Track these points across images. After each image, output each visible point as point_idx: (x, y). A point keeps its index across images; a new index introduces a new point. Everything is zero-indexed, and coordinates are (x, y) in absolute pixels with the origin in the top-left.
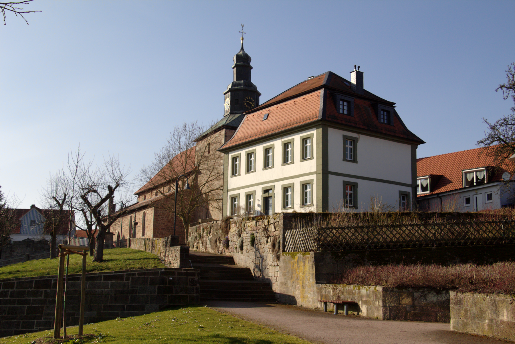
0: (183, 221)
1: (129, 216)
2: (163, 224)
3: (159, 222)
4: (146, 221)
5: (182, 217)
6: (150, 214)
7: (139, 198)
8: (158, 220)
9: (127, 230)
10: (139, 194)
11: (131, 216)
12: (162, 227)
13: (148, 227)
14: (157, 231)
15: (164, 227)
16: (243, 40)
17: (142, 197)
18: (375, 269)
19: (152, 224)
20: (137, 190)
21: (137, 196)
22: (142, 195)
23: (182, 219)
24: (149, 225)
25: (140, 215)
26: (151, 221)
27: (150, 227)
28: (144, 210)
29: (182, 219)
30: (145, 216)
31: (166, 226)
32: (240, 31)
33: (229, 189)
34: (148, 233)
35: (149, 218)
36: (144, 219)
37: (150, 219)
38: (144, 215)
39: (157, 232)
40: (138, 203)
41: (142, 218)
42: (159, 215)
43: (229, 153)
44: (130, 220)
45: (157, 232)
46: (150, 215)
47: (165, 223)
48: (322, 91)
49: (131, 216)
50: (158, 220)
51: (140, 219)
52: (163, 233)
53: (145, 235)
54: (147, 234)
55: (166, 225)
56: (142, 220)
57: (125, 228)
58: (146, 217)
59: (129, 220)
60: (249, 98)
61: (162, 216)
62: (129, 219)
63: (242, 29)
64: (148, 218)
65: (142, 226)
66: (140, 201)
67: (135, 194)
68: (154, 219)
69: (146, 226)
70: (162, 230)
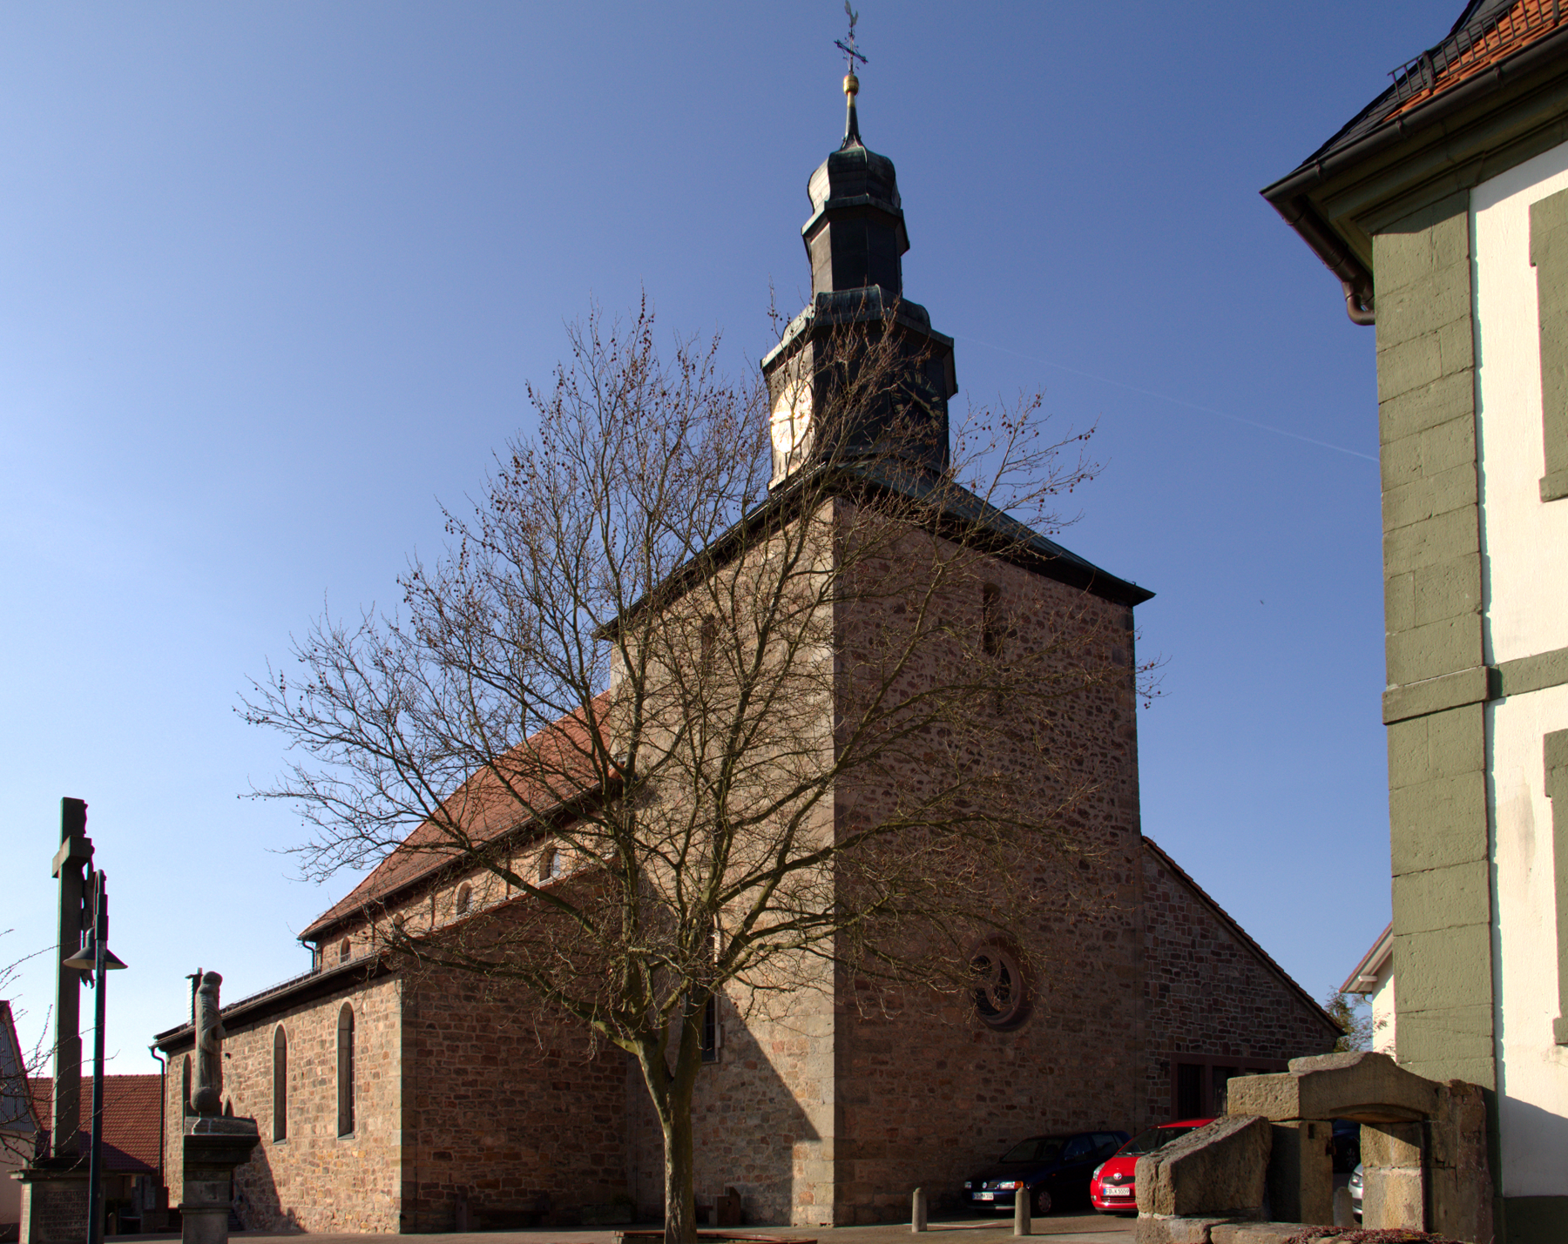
0: (645, 1069)
1: (273, 1027)
2: (459, 1072)
3: (433, 1060)
4: (357, 1056)
5: (639, 1037)
6: (378, 1020)
7: (321, 951)
8: (430, 1053)
9: (262, 1094)
10: (319, 936)
11: (280, 1029)
12: (451, 1089)
13: (373, 1092)
14: (427, 1112)
15: (462, 1091)
16: (854, 90)
17: (333, 949)
18: (1357, 1175)
19: (394, 1074)
20: (308, 918)
21: (313, 945)
22: (331, 941)
23: (638, 1050)
24: (376, 1075)
25: (326, 1023)
26: (386, 1056)
27: (381, 1088)
28: (346, 999)
29: (638, 1050)
30: (351, 1028)
31: (473, 1083)
32: (842, 41)
33: (1501, 656)
34: (370, 1120)
35: (374, 1040)
36: (346, 1043)
37: (382, 1046)
38: (346, 1025)
39: (423, 1117)
40: (315, 973)
41: (336, 1037)
42: (431, 1026)
43: (1478, 192)
44: (277, 1049)
45: (423, 1117)
46: (381, 1025)
47: (469, 1068)
48: (512, 886)
49: (280, 1029)
50: (430, 1053)
51: (323, 1043)
52: (460, 1122)
53: (357, 1128)
54: (365, 1127)
55: (470, 1078)
56: (336, 1047)
57: (257, 1084)
58: (357, 1033)
59: (272, 1049)
60: (919, 380)
61: (448, 1027)
62: (272, 1041)
63: (851, 35)
64: (367, 1041)
65: (335, 1082)
66: (325, 964)
67: (299, 939)
68: (406, 1045)
69: (358, 1082)
70: (452, 1105)
